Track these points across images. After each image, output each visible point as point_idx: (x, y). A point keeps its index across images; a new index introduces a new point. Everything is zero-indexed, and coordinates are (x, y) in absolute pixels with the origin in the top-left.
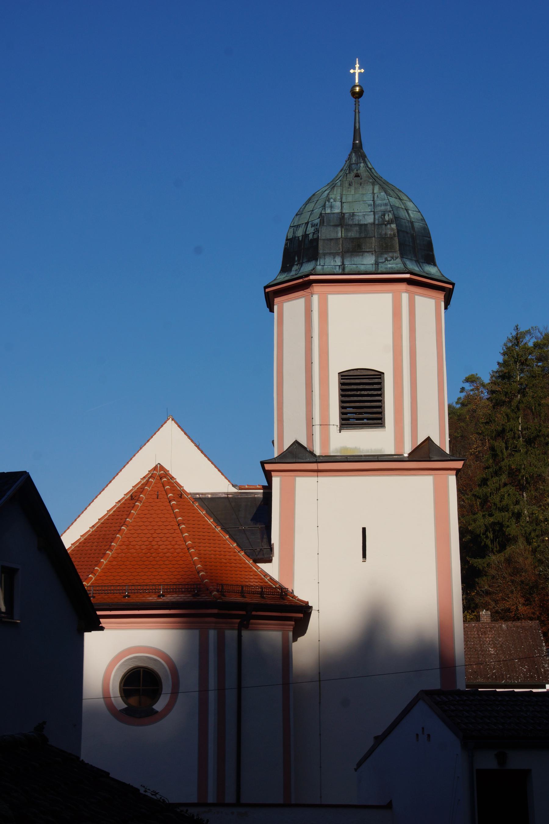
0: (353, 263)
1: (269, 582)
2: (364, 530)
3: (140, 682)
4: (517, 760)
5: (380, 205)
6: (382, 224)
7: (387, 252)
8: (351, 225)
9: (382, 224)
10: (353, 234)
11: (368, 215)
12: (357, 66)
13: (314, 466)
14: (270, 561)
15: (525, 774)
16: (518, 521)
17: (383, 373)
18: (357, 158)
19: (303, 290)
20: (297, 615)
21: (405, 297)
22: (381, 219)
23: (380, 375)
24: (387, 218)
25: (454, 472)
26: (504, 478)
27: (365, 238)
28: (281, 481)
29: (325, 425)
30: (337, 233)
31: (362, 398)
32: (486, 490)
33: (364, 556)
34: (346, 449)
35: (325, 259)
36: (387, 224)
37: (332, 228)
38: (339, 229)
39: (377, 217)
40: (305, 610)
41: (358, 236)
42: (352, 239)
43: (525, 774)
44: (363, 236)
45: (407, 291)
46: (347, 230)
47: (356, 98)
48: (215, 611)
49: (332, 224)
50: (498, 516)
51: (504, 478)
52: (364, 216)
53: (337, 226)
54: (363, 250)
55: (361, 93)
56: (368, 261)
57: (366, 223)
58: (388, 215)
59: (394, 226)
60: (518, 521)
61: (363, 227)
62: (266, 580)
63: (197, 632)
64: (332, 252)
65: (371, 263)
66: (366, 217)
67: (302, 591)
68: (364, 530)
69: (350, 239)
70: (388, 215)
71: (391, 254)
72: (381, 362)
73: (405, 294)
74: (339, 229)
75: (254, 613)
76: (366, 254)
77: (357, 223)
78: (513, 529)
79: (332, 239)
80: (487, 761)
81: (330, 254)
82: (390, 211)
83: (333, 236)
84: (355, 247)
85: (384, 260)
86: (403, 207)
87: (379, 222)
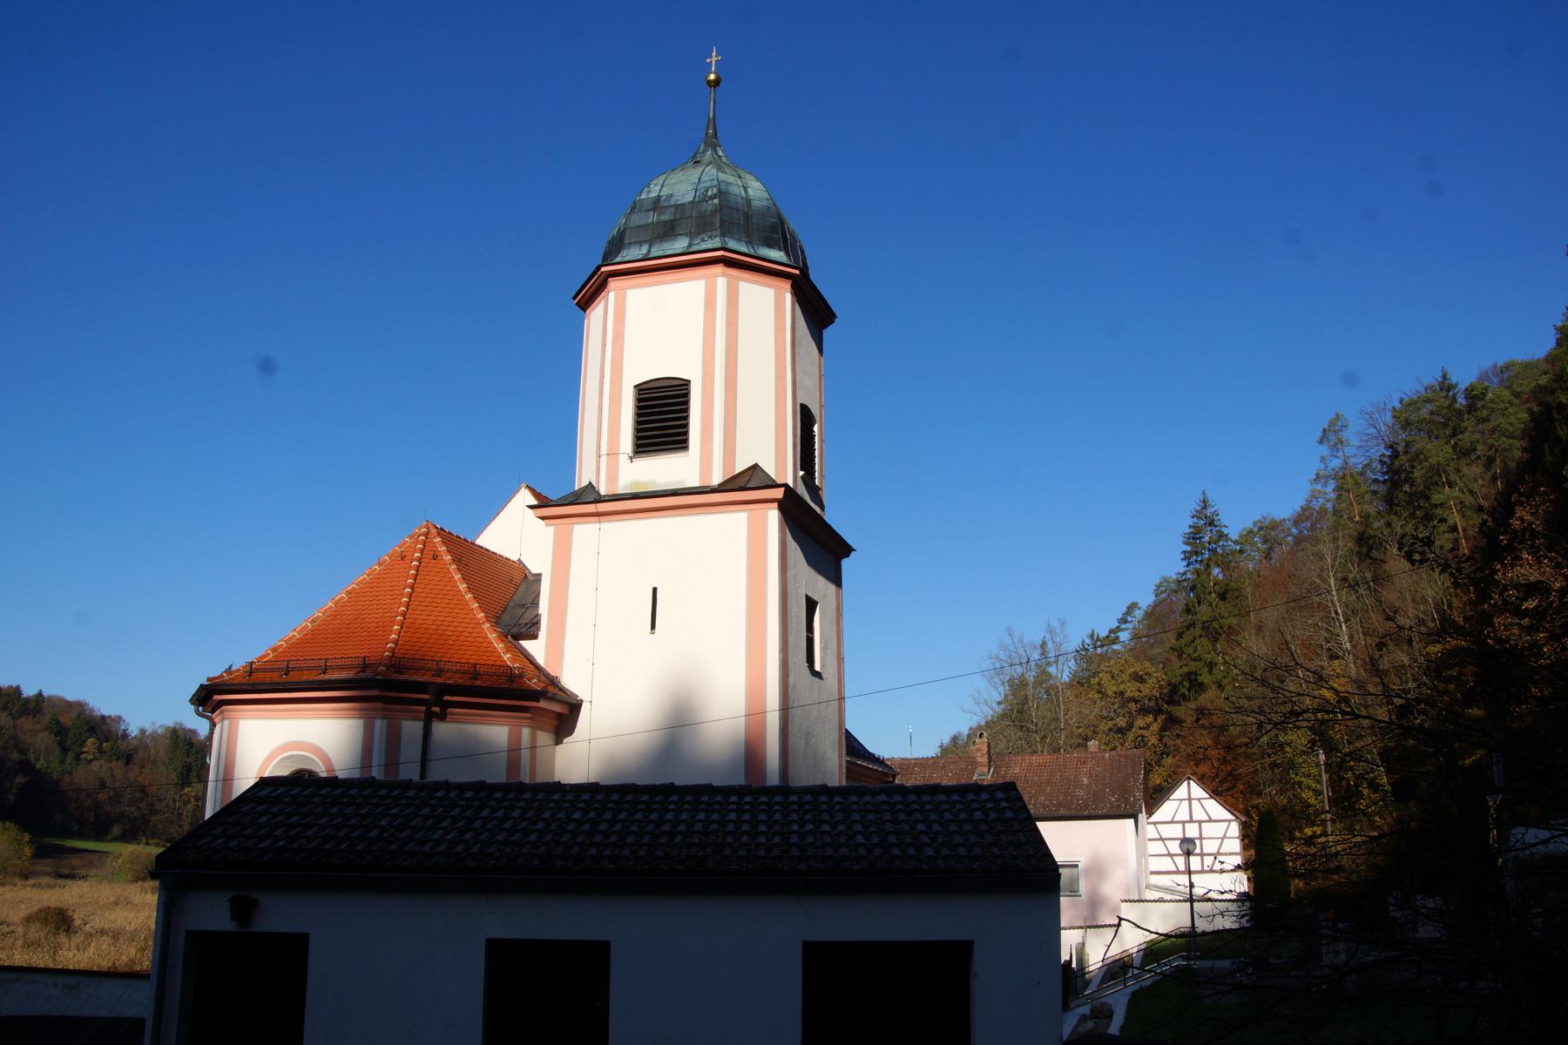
2: (655, 590)
3: (1298, 891)
4: (280, 914)
13: (591, 508)
14: (535, 637)
15: (299, 943)
16: (1210, 671)
20: (564, 714)
21: (722, 283)
23: (687, 383)
26: (1197, 631)
29: (613, 454)
31: (662, 416)
32: (1182, 642)
33: (653, 627)
34: (638, 483)
40: (574, 707)
42: (665, 222)
43: (299, 943)
45: (724, 275)
46: (660, 214)
48: (375, 693)
50: (1193, 666)
51: (1197, 631)
56: (681, 244)
60: (1210, 671)
61: (679, 207)
63: (360, 723)
67: (572, 680)
68: (655, 590)
73: (721, 278)
75: (447, 698)
78: (1205, 678)
80: (212, 913)
83: (643, 222)
84: (668, 231)
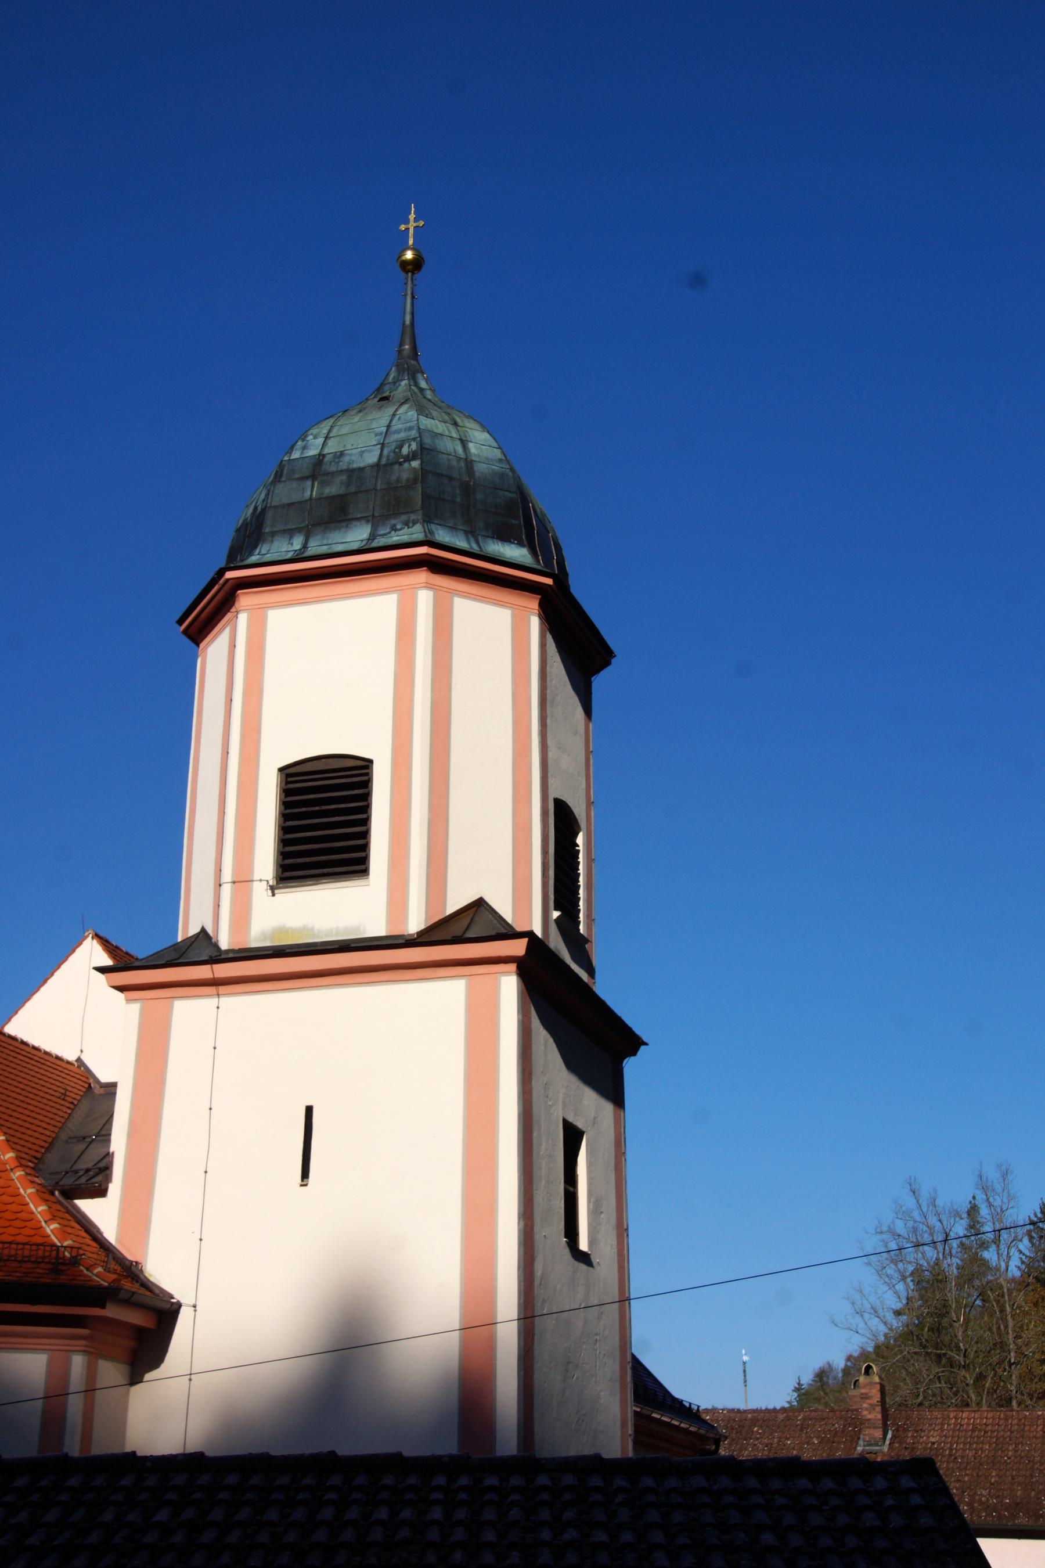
0: (325, 542)
1: (53, 1237)
2: (309, 1110)
5: (399, 431)
6: (392, 464)
7: (396, 515)
8: (332, 474)
9: (392, 464)
10: (332, 490)
11: (369, 451)
12: (412, 216)
13: (203, 972)
14: (101, 1192)
17: (371, 761)
18: (399, 373)
19: (228, 611)
20: (140, 1322)
21: (425, 599)
22: (392, 455)
23: (366, 765)
24: (405, 451)
25: (513, 967)
27: (356, 493)
28: (143, 1013)
29: (243, 882)
30: (303, 490)
31: (325, 818)
33: (305, 1173)
34: (282, 930)
35: (272, 542)
36: (404, 462)
37: (295, 485)
38: (309, 483)
39: (385, 452)
40: (164, 1314)
41: (342, 491)
42: (331, 499)
44: (353, 490)
45: (428, 586)
46: (323, 484)
47: (407, 272)
49: (297, 476)
52: (361, 453)
53: (304, 478)
54: (350, 516)
55: (416, 265)
57: (362, 465)
58: (410, 445)
59: (415, 464)
61: (355, 474)
62: (48, 1231)
64: (290, 527)
65: (361, 538)
66: (365, 455)
67: (164, 1268)
68: (309, 1110)
69: (327, 498)
70: (410, 445)
71: (404, 518)
72: (363, 736)
73: (423, 592)
74: (309, 483)
76: (355, 523)
77: (345, 467)
79: (292, 504)
81: (284, 532)
82: (414, 439)
83: (295, 497)
84: (337, 513)
85: (388, 530)
86: (454, 435)
87: (388, 459)
